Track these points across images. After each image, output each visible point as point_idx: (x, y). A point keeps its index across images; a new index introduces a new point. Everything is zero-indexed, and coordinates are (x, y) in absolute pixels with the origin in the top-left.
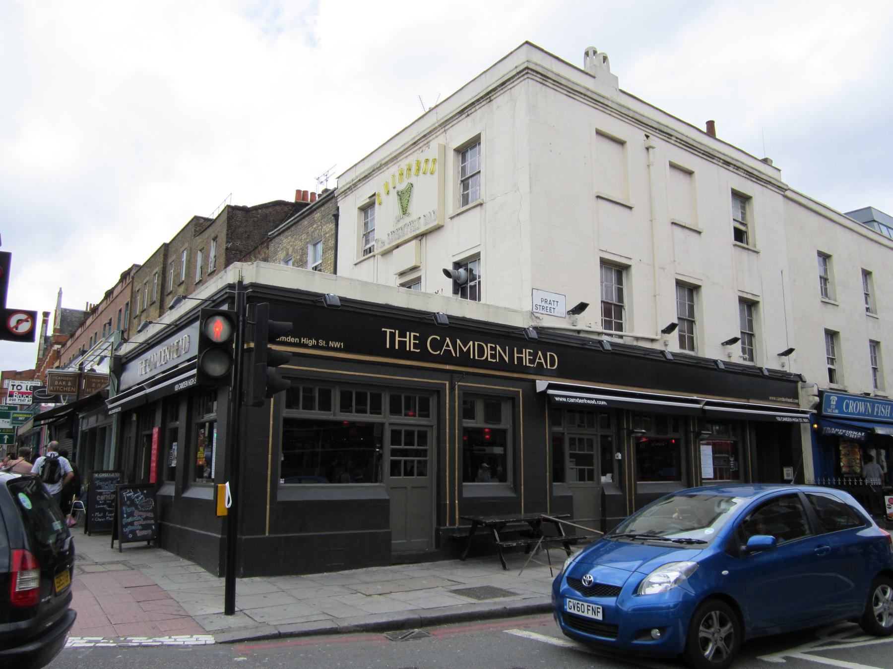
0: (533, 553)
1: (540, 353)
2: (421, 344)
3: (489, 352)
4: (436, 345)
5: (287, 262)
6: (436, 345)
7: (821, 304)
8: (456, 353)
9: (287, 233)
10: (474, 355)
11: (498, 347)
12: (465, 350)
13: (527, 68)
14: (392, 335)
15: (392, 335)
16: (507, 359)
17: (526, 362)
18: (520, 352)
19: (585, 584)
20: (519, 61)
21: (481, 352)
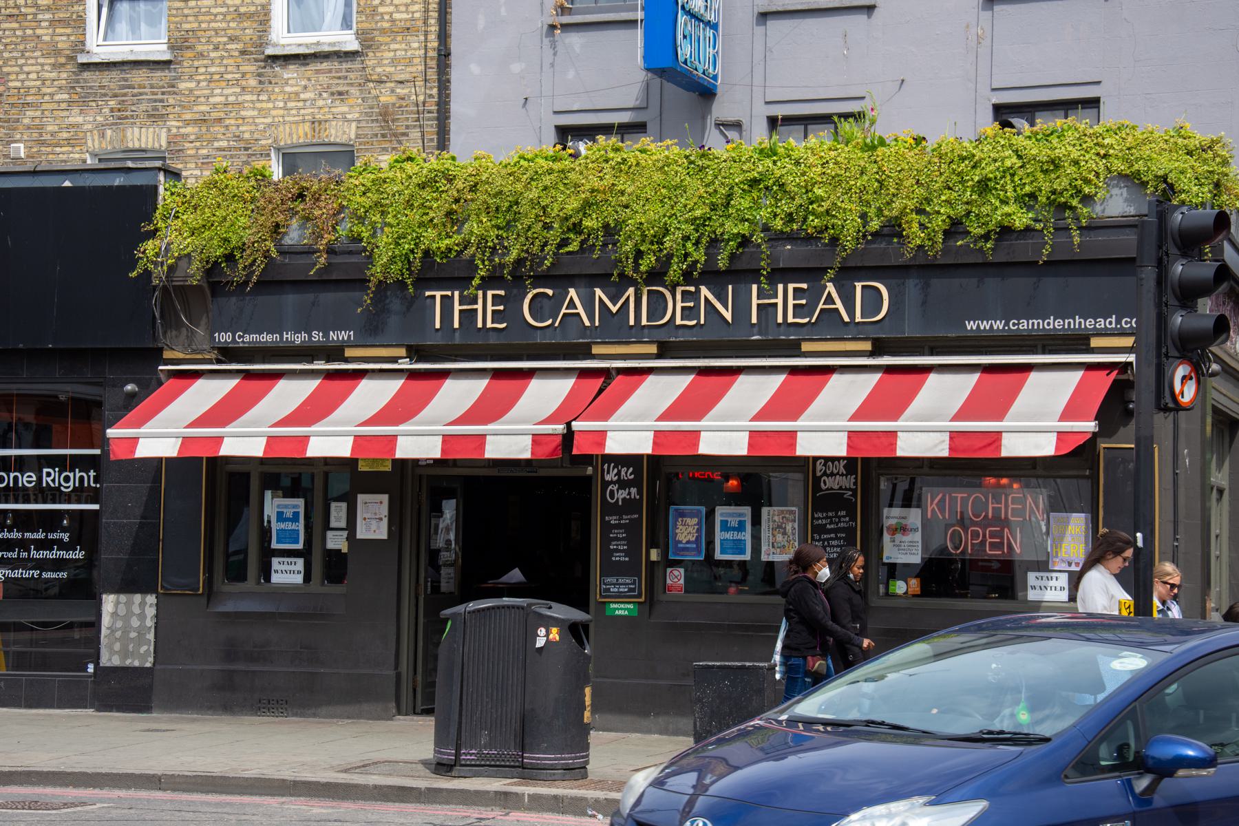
3: (679, 305)
11: (704, 291)
12: (614, 309)
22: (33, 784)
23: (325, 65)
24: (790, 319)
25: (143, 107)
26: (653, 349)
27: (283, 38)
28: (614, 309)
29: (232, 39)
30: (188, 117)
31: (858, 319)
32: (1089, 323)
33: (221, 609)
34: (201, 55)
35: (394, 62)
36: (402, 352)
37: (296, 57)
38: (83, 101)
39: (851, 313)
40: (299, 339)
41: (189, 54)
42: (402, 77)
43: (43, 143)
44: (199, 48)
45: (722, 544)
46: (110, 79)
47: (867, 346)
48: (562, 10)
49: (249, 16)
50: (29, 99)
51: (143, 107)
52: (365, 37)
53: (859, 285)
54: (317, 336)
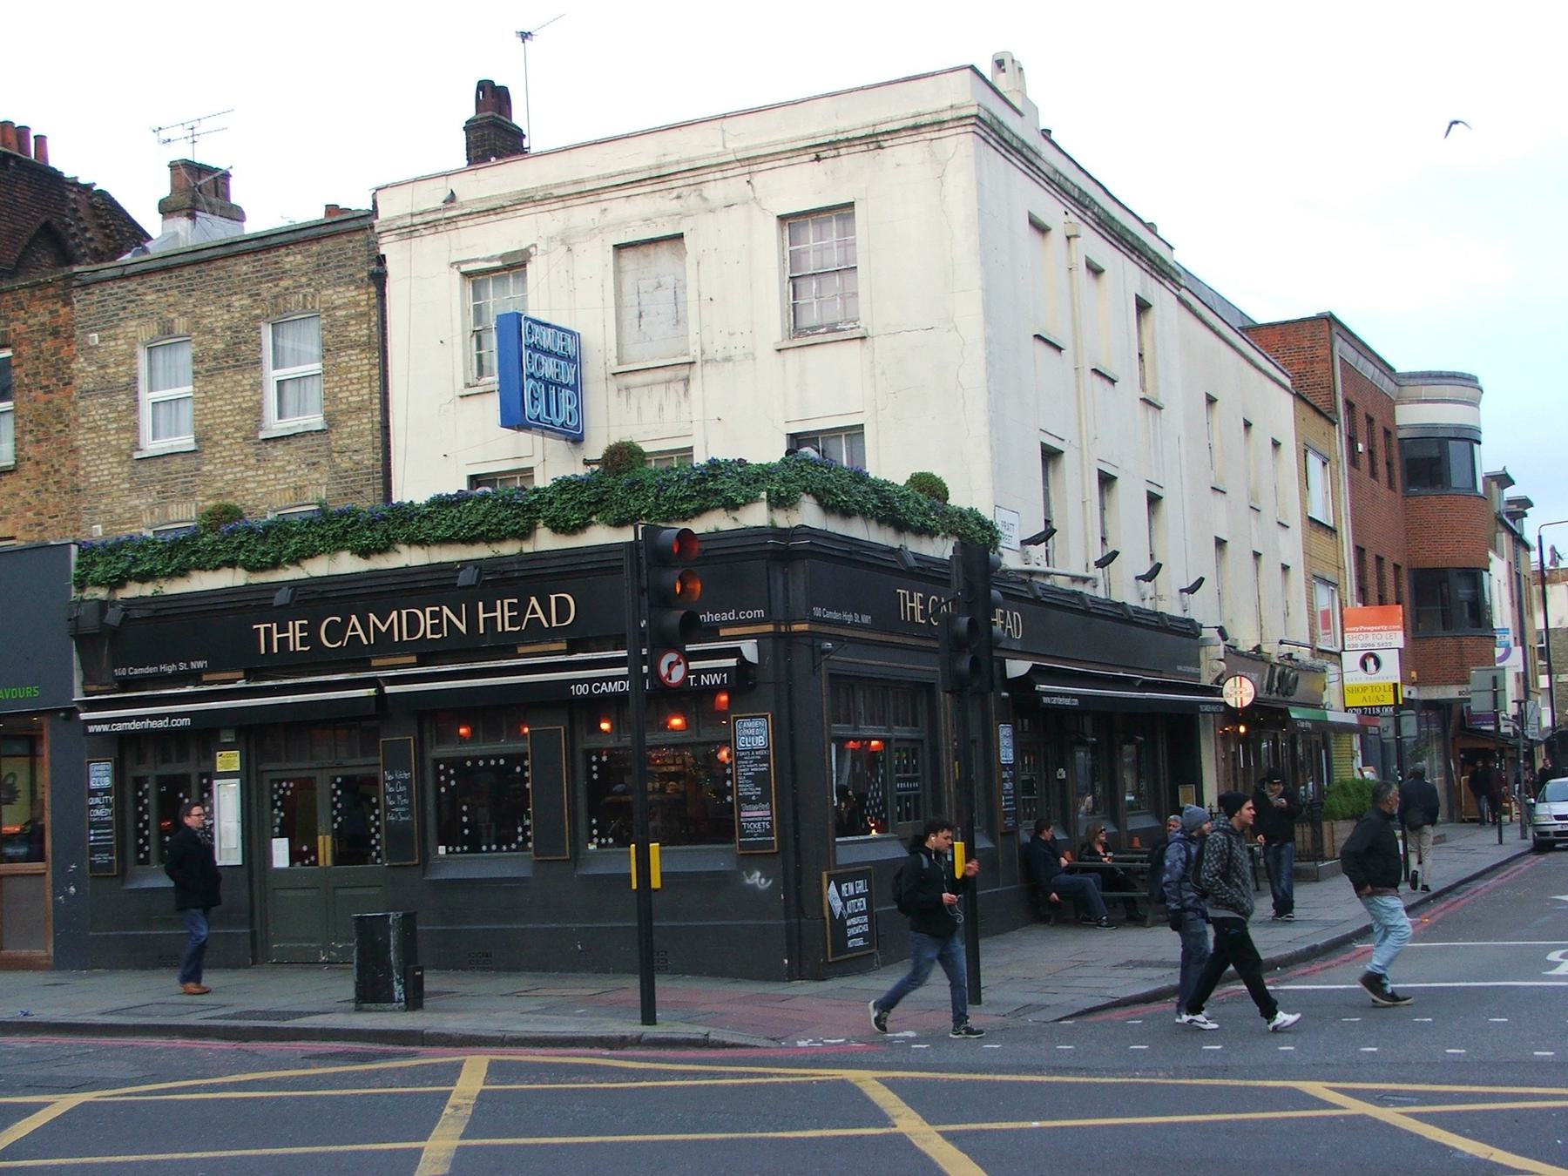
0: (230, 501)
1: (534, 600)
2: (311, 638)
3: (429, 622)
4: (335, 632)
5: (74, 451)
6: (335, 632)
7: (1139, 406)
8: (549, 622)
9: (156, 279)
10: (401, 634)
11: (446, 610)
12: (384, 629)
13: (977, 116)
14: (268, 631)
15: (268, 631)
16: (463, 628)
17: (295, 645)
18: (489, 608)
19: (228, 737)
20: (974, 111)
21: (413, 622)
22: (112, 1035)
23: (302, 443)
24: (507, 628)
25: (179, 487)
26: (413, 659)
27: (274, 425)
28: (384, 629)
29: (238, 429)
30: (210, 492)
31: (554, 624)
32: (717, 617)
33: (135, 886)
34: (216, 444)
35: (350, 435)
36: (241, 674)
37: (282, 438)
38: (138, 487)
39: (549, 622)
40: (170, 669)
41: (208, 444)
42: (356, 447)
43: (113, 523)
44: (215, 438)
45: (42, 849)
46: (156, 470)
47: (413, 659)
48: (468, 385)
49: (249, 410)
50: (104, 490)
51: (179, 487)
52: (330, 419)
53: (553, 597)
54: (183, 666)
